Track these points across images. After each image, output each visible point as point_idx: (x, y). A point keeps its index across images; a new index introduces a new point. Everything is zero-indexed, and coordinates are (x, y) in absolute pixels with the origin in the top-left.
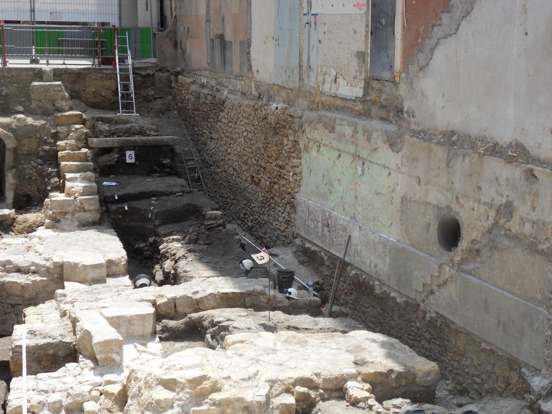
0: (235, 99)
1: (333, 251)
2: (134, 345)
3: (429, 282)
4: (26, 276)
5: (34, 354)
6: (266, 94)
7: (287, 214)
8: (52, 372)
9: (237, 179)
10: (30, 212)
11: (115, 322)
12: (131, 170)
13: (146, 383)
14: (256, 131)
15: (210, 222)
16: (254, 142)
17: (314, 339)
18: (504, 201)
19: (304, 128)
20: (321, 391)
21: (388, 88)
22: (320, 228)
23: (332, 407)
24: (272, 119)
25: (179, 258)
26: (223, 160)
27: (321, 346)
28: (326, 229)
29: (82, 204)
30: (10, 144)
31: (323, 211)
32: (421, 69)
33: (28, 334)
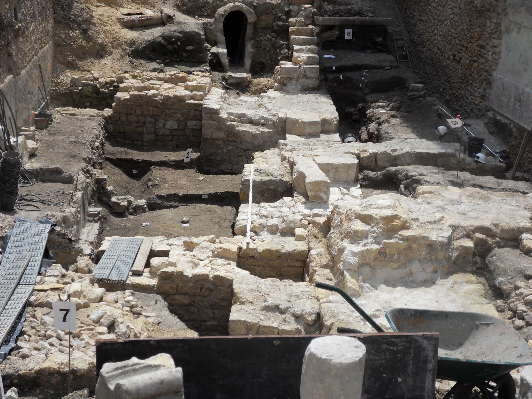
1: (522, 124)
2: (339, 188)
5: (259, 188)
7: (482, 90)
8: (272, 202)
9: (440, 57)
10: (263, 77)
11: (324, 167)
12: (348, 45)
13: (347, 216)
14: (462, 14)
15: (412, 93)
16: (459, 24)
17: (496, 197)
19: (507, 11)
20: (498, 239)
22: (512, 103)
23: (507, 253)
25: (383, 122)
26: (429, 40)
27: (502, 202)
28: (518, 104)
29: (305, 72)
31: (517, 88)
33: (255, 171)
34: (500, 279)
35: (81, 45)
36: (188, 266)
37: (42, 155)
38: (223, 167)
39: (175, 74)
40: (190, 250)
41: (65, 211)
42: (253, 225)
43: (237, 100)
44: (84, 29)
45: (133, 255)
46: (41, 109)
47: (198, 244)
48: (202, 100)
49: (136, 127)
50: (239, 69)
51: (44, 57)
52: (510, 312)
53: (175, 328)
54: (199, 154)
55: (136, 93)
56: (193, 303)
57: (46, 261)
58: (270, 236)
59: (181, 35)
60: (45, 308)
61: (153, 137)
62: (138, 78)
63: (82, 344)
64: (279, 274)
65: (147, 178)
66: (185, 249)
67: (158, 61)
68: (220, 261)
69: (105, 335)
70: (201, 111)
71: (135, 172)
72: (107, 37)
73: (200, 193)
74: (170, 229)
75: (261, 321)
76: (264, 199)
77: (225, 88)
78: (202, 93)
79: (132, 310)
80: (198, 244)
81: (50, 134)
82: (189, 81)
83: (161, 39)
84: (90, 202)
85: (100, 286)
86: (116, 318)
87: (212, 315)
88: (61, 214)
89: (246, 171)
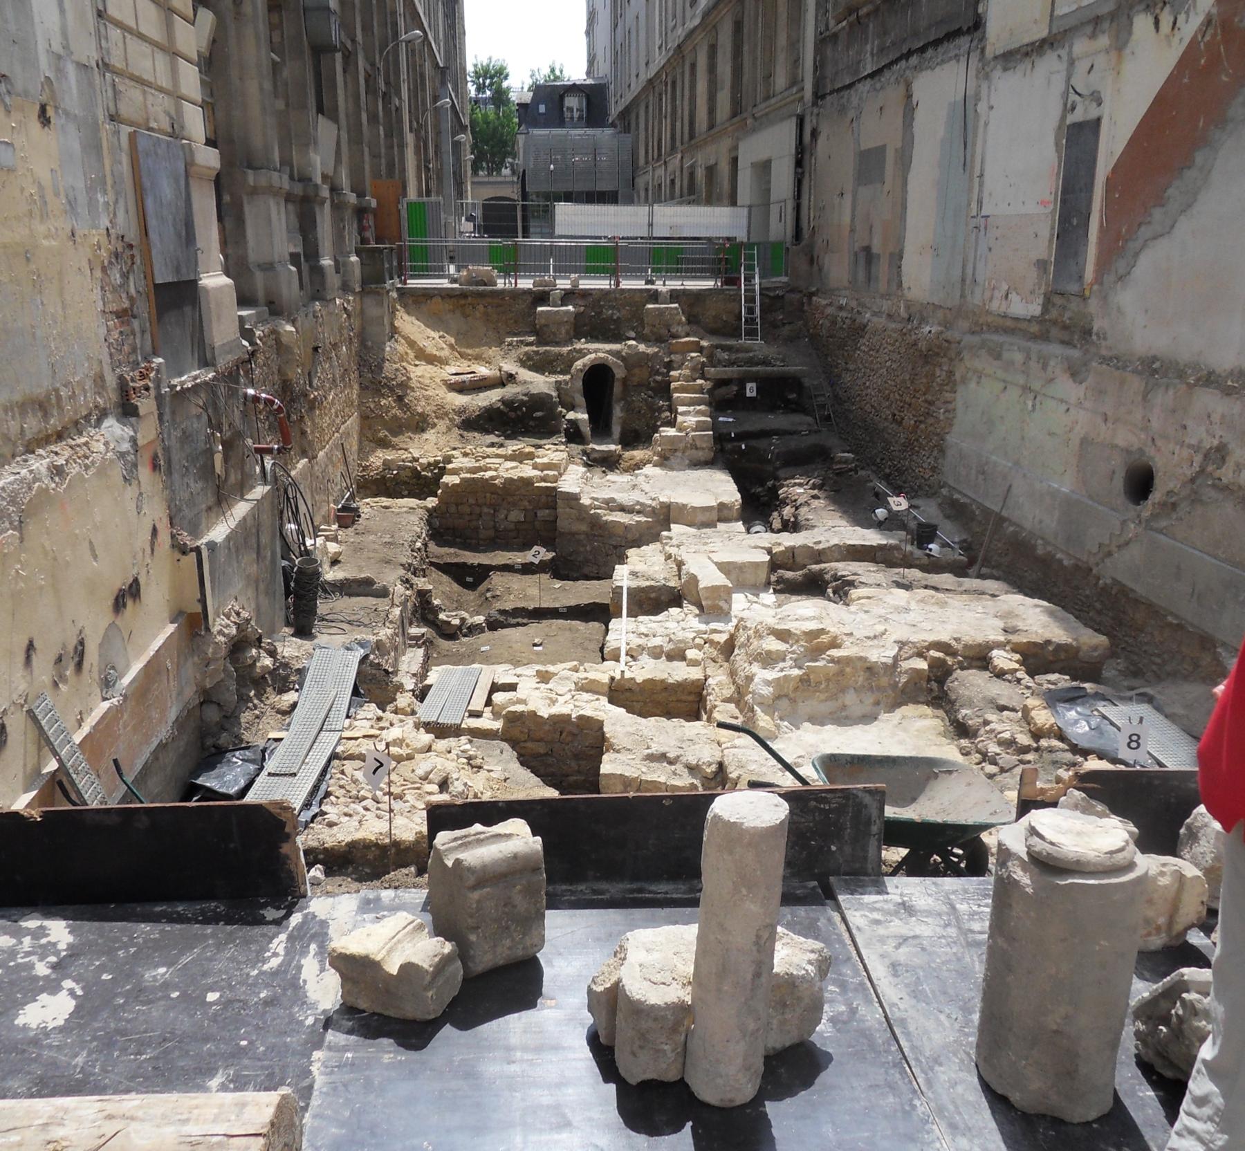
0: (880, 322)
1: (988, 504)
3: (1107, 542)
4: (630, 515)
6: (917, 315)
11: (725, 568)
12: (751, 405)
13: (757, 631)
17: (956, 601)
18: (1216, 442)
20: (960, 658)
21: (1074, 305)
24: (923, 345)
28: (981, 477)
30: (619, 373)
32: (1120, 278)
34: (964, 712)
52: (978, 756)
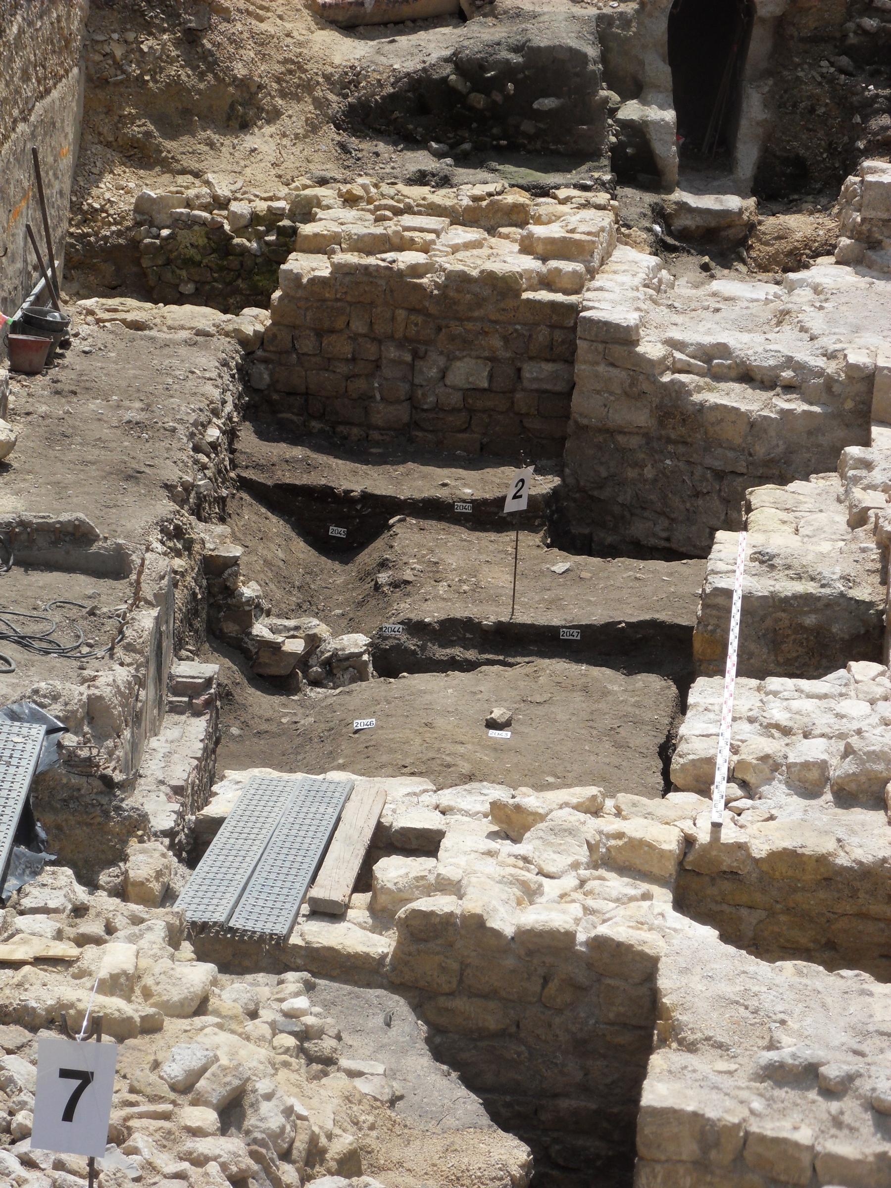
5: (763, 619)
10: (799, 211)
33: (752, 560)
35: (175, 84)
36: (504, 896)
37: (27, 466)
38: (639, 529)
39: (490, 195)
40: (512, 834)
41: (94, 679)
42: (736, 758)
43: (700, 292)
44: (189, 29)
45: (316, 841)
46: (33, 304)
47: (542, 817)
48: (577, 292)
49: (348, 378)
50: (714, 179)
51: (49, 125)
53: (450, 1121)
54: (557, 481)
55: (352, 258)
56: (513, 1029)
57: (24, 854)
58: (797, 803)
59: (521, 60)
60: (12, 1027)
61: (402, 413)
62: (363, 205)
63: (130, 1167)
64: (823, 941)
65: (375, 555)
66: (496, 828)
67: (434, 145)
68: (616, 884)
69: (209, 1139)
70: (574, 329)
71: (337, 531)
72: (264, 57)
73: (556, 622)
74: (450, 747)
75: (752, 1119)
76: (781, 660)
77: (661, 248)
78: (579, 267)
79: (306, 1045)
80: (542, 817)
81: (58, 393)
82: (538, 221)
83: (448, 69)
84: (181, 640)
85: (202, 956)
86: (248, 1079)
87: (579, 1076)
88: (83, 688)
89: (722, 555)
